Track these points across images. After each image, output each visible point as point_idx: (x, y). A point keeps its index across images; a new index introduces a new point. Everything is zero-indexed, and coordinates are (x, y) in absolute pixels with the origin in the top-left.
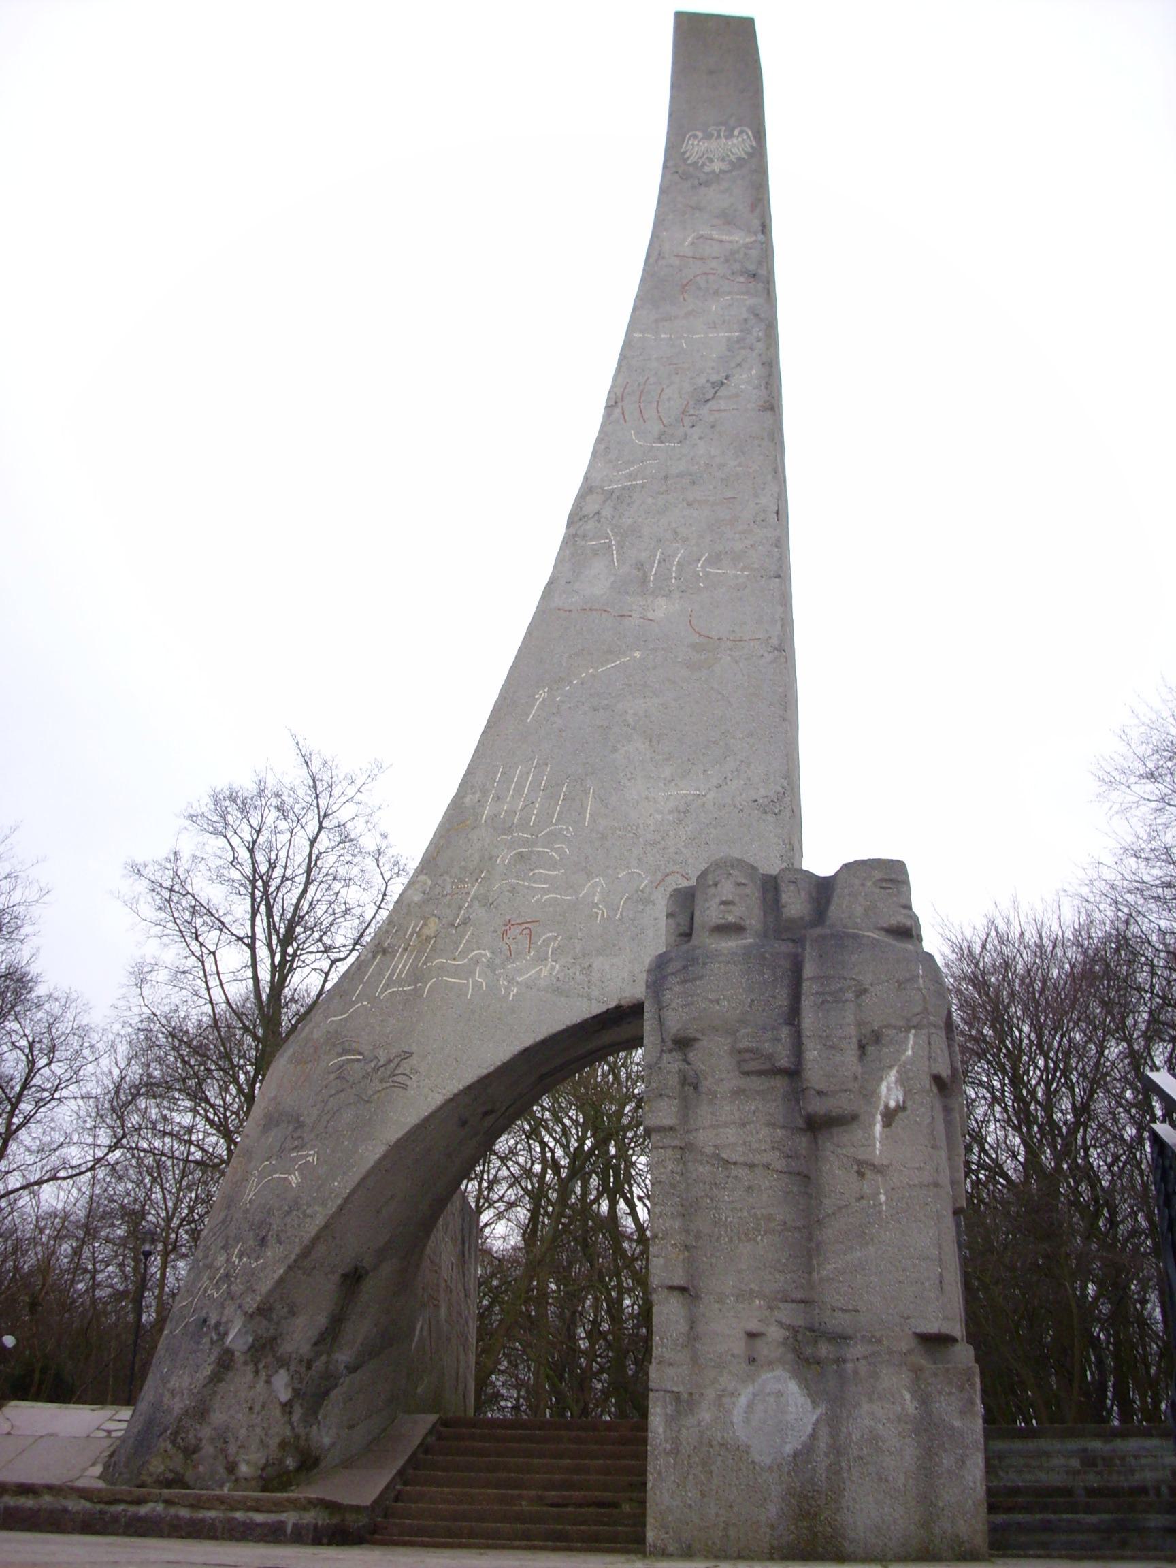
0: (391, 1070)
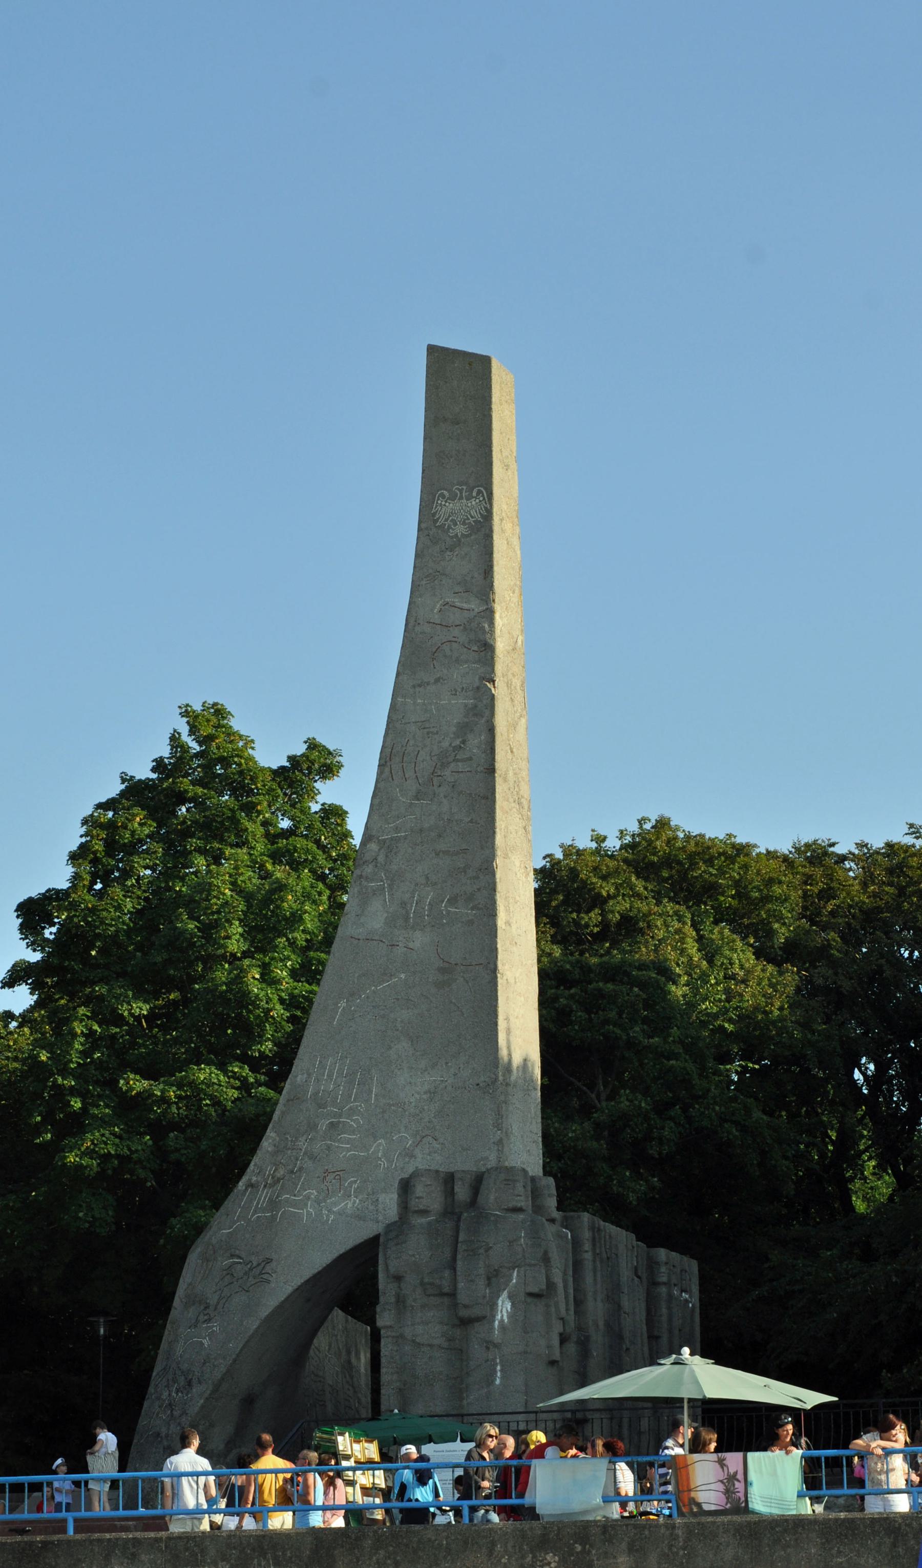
0: (259, 1271)
